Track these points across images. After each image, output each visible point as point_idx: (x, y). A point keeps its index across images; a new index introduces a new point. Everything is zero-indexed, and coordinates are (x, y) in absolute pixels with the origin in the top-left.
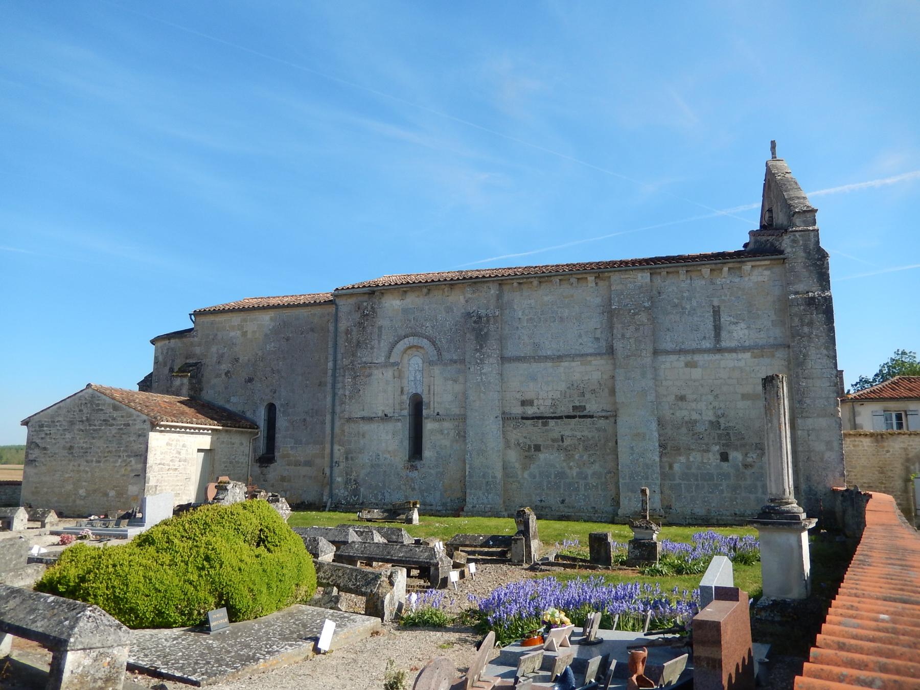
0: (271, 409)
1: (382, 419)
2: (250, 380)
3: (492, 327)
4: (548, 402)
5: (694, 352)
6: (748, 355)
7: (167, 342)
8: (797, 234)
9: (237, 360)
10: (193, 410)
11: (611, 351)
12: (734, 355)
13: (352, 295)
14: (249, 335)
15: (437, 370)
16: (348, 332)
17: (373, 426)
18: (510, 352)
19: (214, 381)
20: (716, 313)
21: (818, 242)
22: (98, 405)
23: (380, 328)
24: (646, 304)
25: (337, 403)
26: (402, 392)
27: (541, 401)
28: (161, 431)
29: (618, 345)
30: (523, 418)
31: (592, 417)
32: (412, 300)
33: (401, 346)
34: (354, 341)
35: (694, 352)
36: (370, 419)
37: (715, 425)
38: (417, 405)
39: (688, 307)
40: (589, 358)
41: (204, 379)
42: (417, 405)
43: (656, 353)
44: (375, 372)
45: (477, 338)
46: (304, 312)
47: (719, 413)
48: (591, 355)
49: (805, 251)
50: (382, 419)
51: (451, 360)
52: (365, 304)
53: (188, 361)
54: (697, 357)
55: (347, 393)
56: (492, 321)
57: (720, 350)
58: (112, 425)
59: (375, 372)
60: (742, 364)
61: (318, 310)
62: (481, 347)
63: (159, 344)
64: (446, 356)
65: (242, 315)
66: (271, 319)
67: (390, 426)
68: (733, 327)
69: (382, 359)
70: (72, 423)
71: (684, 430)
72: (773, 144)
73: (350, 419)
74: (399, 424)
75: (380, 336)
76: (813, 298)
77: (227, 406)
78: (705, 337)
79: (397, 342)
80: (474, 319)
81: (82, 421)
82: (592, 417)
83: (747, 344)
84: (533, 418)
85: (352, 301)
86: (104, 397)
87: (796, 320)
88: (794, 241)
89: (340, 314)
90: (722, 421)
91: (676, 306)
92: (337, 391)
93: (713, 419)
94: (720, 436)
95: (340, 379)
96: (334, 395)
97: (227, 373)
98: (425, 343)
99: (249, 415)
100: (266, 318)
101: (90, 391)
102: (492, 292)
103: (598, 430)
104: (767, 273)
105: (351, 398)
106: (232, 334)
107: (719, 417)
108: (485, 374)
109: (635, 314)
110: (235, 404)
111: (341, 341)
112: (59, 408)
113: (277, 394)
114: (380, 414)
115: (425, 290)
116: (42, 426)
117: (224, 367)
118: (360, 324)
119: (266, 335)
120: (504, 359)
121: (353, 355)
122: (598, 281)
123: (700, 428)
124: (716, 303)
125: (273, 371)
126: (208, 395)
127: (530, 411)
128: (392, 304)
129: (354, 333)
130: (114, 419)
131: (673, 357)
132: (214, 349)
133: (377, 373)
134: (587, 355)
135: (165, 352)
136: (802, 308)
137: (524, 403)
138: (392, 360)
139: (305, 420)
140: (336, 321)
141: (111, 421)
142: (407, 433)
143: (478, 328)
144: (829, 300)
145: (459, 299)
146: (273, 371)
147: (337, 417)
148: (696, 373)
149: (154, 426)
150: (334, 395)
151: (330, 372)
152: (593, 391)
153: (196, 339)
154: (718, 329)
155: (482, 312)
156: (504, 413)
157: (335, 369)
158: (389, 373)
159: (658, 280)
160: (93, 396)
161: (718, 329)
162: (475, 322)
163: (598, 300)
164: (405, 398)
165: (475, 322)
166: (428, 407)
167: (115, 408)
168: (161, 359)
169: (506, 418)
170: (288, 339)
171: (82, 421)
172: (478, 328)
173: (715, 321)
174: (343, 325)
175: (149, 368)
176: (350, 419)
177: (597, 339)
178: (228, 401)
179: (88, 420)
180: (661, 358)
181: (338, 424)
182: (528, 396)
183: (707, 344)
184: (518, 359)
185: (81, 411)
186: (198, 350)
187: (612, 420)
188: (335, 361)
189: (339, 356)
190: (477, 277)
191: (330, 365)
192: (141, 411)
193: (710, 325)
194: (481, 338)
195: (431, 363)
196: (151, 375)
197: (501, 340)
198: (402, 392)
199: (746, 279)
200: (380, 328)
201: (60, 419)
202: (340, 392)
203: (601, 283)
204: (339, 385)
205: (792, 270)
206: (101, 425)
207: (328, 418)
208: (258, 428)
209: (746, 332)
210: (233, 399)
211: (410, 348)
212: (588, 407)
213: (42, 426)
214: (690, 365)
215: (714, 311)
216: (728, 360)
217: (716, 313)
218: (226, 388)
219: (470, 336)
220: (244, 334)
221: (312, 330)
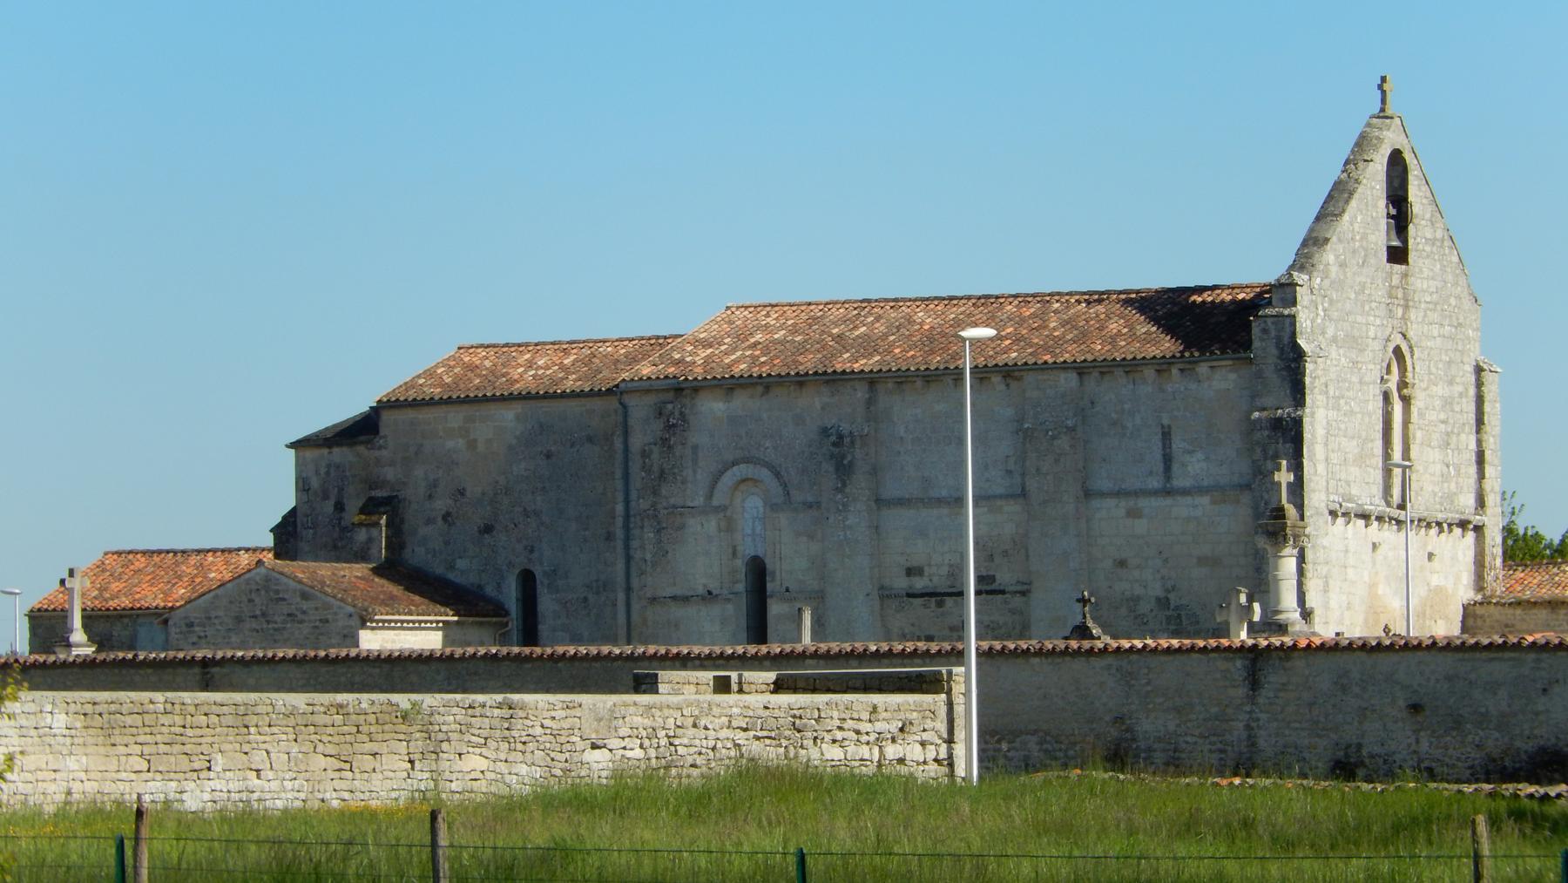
0: (528, 580)
1: (703, 598)
2: (488, 529)
3: (858, 453)
4: (945, 570)
5: (1137, 493)
6: (1205, 500)
7: (325, 451)
8: (1269, 321)
9: (462, 492)
10: (741, 864)
11: (1024, 494)
12: (1189, 500)
13: (648, 391)
14: (481, 448)
15: (783, 519)
16: (645, 454)
17: (690, 611)
18: (890, 490)
19: (424, 531)
20: (1166, 435)
21: (1294, 334)
22: (277, 592)
23: (695, 448)
24: (1070, 423)
25: (634, 570)
26: (734, 554)
27: (934, 569)
28: (373, 629)
29: (1032, 484)
30: (909, 595)
31: (1003, 592)
32: (742, 402)
33: (728, 479)
34: (656, 468)
35: (1137, 493)
36: (685, 599)
37: (1163, 603)
38: (758, 572)
39: (1130, 425)
40: (999, 503)
41: (406, 527)
42: (758, 572)
43: (1088, 494)
44: (691, 521)
45: (837, 470)
46: (573, 405)
47: (1169, 584)
48: (1001, 497)
49: (1277, 346)
50: (703, 598)
51: (804, 503)
52: (670, 406)
53: (373, 493)
54: (1143, 503)
55: (648, 556)
56: (858, 443)
57: (1168, 492)
58: (301, 622)
59: (691, 521)
60: (1198, 512)
61: (597, 404)
62: (844, 485)
63: (310, 454)
64: (798, 497)
65: (465, 410)
66: (517, 418)
67: (716, 610)
68: (1187, 458)
69: (699, 501)
70: (239, 620)
71: (1124, 611)
72: (1383, 79)
73: (653, 600)
74: (730, 607)
75: (695, 461)
76: (1280, 420)
77: (451, 576)
78: (1151, 473)
79: (721, 473)
80: (833, 438)
81: (255, 617)
82: (1003, 592)
83: (1205, 483)
84: (922, 595)
85: (651, 399)
86: (285, 580)
87: (1258, 450)
88: (1265, 331)
89: (631, 422)
90: (1172, 596)
91: (1114, 424)
92: (632, 552)
93: (1161, 594)
94: (1169, 618)
95: (636, 532)
96: (628, 559)
97: (446, 517)
98: (765, 473)
99: (490, 590)
100: (508, 415)
101: (262, 570)
102: (859, 395)
103: (1013, 612)
104: (1233, 376)
105: (654, 565)
106: (450, 444)
107: (1168, 591)
108: (850, 527)
109: (1054, 438)
110: (465, 571)
111: (635, 467)
112: (216, 596)
113: (536, 555)
114: (701, 590)
115: (760, 389)
116: (191, 625)
117: (441, 504)
118: (664, 441)
119: (510, 448)
120: (879, 501)
121: (655, 493)
122: (1009, 381)
123: (1144, 607)
124: (1166, 422)
125: (526, 513)
126: (416, 555)
127: (919, 584)
128: (713, 407)
129: (655, 456)
130: (304, 612)
131: (1110, 502)
132: (419, 472)
133: (693, 524)
134: (995, 497)
135: (323, 471)
136: (1266, 433)
137: (910, 572)
138: (715, 502)
139: (586, 599)
140: (626, 433)
141: (300, 616)
142: (743, 622)
143: (839, 453)
144: (1298, 423)
145: (814, 402)
146: (526, 513)
147: (634, 596)
148: (1141, 526)
149: (363, 626)
150: (628, 559)
151: (619, 521)
152: (1005, 553)
153: (384, 453)
154: (1168, 460)
155: (845, 428)
156: (882, 588)
157: (627, 516)
158: (712, 524)
159: (422, 779)
160: (267, 579)
161: (1168, 460)
162: (834, 444)
163: (1009, 412)
164: (740, 563)
165: (834, 444)
166: (773, 580)
167: (305, 596)
168: (315, 483)
169: (885, 595)
170: (548, 456)
171: (255, 617)
172: (839, 453)
173: (1164, 447)
174: (637, 442)
175: (285, 499)
176: (653, 600)
177: (1009, 472)
178: (452, 567)
179: (264, 615)
180: (1096, 503)
181: (635, 607)
182: (915, 562)
183: (1155, 483)
184: (901, 502)
185: (250, 601)
186: (390, 474)
187: (1376, 504)
188: (627, 502)
189: (634, 495)
190: (844, 372)
191: (620, 508)
192: (342, 600)
193: (1158, 455)
194: (844, 470)
195: (774, 507)
196: (293, 512)
197: (874, 471)
198: (734, 554)
199: (1206, 385)
200: (695, 448)
201: (221, 613)
202: (637, 555)
203: (1014, 385)
204: (635, 544)
205: (1259, 375)
206: (284, 622)
207: (621, 596)
208: (507, 613)
209: (1204, 465)
210: (461, 564)
211: (744, 481)
212: (998, 577)
213: (191, 625)
214: (1133, 513)
215: (1164, 434)
216: (1182, 507)
217: (1166, 435)
218: (447, 543)
219: (828, 467)
220: (472, 444)
221: (590, 439)
